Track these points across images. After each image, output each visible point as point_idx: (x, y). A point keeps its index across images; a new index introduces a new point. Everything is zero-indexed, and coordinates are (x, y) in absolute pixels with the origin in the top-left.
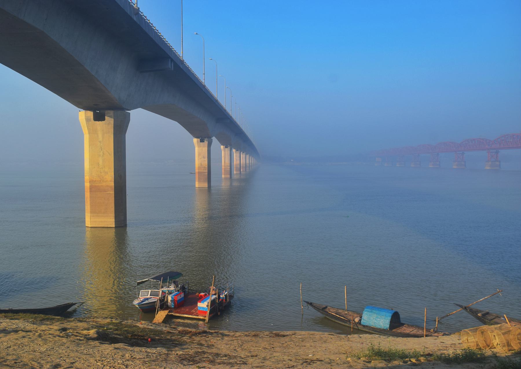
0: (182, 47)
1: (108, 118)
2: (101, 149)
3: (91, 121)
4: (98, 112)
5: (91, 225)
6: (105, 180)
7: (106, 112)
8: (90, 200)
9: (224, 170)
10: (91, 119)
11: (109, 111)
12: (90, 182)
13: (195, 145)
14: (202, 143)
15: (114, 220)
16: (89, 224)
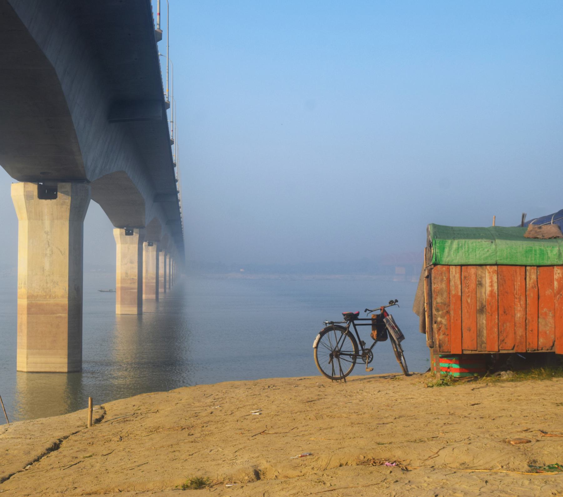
0: (167, 82)
1: (62, 194)
2: (49, 244)
3: (33, 199)
4: (42, 184)
5: (27, 368)
6: (54, 296)
7: (60, 185)
8: (28, 328)
9: (146, 285)
10: (33, 195)
11: (64, 184)
12: (28, 298)
13: (116, 240)
14: (128, 237)
15: (66, 360)
16: (25, 365)
